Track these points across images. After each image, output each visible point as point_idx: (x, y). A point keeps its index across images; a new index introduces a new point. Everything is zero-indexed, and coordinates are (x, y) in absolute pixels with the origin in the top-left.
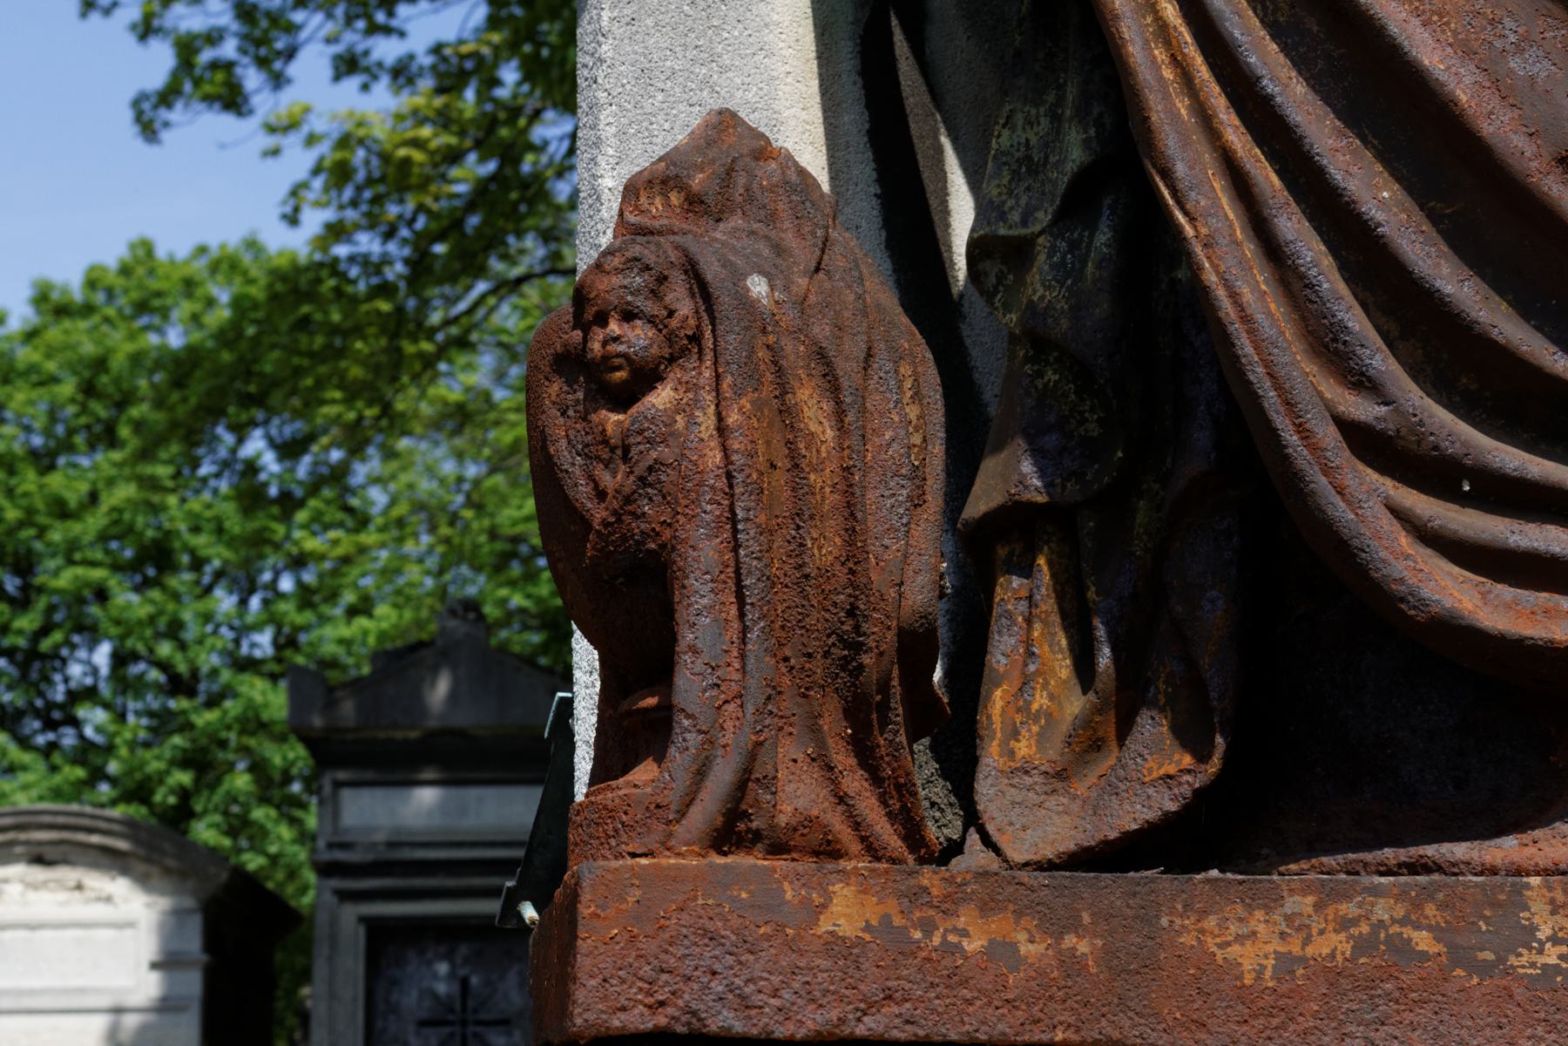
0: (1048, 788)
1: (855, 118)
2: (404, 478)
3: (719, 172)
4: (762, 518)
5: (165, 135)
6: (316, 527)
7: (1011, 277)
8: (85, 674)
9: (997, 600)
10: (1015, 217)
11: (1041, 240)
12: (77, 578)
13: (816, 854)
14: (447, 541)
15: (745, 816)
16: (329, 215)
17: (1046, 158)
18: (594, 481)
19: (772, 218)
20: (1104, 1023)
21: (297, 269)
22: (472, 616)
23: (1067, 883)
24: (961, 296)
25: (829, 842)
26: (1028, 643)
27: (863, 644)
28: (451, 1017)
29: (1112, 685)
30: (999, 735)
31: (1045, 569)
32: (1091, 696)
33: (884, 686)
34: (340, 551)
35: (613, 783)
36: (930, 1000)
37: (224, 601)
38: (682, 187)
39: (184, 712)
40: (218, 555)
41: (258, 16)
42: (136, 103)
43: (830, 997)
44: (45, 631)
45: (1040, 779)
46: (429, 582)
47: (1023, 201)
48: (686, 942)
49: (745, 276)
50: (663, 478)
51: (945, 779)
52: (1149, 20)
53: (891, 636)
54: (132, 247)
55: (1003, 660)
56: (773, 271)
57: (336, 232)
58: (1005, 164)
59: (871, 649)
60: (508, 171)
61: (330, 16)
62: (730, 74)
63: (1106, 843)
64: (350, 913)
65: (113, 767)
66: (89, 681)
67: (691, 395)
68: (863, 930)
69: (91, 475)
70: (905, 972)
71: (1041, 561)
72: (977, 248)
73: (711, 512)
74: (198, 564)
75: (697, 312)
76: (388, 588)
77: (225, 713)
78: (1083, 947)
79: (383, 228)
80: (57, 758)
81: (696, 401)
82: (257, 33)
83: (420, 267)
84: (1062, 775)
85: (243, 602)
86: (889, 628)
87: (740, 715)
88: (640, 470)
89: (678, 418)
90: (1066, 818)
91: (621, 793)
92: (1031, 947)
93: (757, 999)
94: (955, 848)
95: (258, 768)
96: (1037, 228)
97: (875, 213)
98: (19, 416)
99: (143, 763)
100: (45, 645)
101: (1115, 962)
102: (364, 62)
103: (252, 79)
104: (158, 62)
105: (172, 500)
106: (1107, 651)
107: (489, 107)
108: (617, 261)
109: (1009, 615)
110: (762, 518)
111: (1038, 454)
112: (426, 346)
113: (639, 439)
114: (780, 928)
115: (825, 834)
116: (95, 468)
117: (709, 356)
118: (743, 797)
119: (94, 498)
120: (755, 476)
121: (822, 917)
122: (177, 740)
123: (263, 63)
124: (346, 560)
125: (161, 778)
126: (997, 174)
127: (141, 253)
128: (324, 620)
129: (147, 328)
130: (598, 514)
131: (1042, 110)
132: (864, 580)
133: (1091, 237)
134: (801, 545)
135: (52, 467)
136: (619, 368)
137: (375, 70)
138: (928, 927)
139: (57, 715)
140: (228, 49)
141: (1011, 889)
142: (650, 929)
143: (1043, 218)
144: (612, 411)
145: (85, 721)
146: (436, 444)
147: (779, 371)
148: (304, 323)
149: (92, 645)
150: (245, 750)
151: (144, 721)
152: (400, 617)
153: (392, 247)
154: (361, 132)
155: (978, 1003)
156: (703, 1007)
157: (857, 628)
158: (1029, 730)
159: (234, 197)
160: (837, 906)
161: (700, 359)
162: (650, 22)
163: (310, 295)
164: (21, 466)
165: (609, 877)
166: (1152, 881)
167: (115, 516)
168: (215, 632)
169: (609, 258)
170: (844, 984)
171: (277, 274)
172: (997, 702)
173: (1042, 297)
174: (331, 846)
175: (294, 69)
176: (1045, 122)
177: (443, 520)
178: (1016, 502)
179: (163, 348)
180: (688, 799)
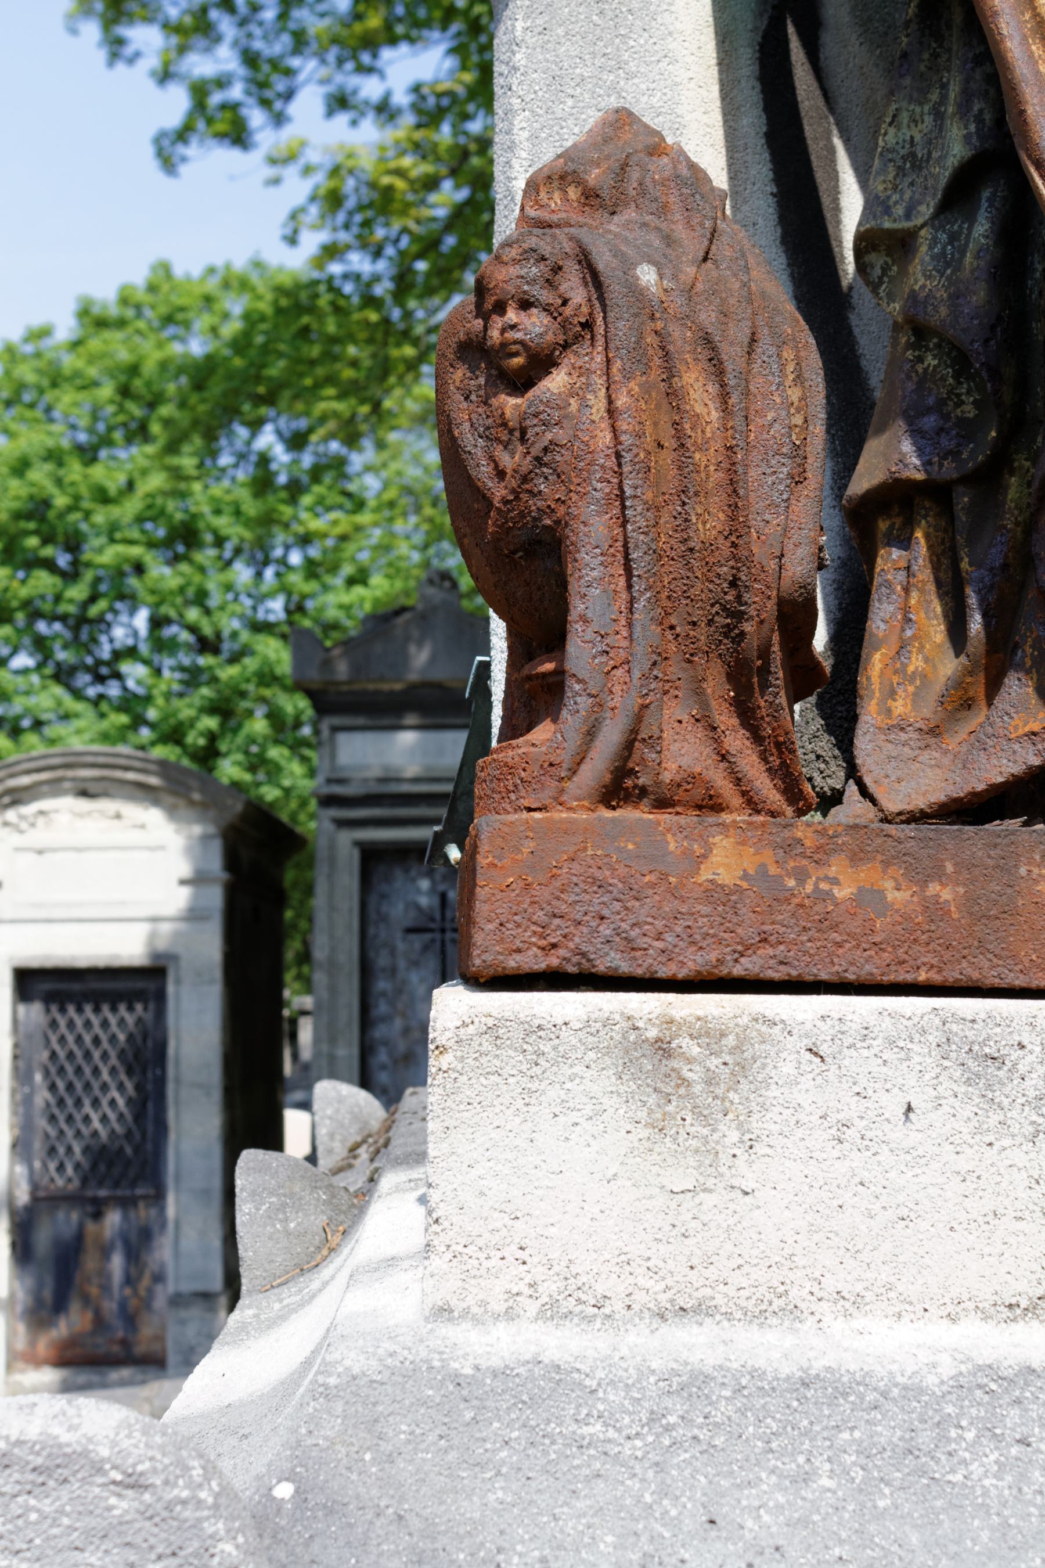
0: (922, 744)
1: (753, 121)
2: (394, 466)
3: (617, 168)
4: (649, 496)
5: (183, 169)
6: (319, 509)
7: (895, 268)
8: (127, 636)
9: (878, 570)
10: (899, 211)
11: (923, 233)
12: (117, 555)
13: (699, 807)
14: (430, 520)
15: (632, 772)
16: (323, 237)
17: (930, 153)
18: (494, 461)
19: (663, 210)
20: (964, 964)
21: (298, 286)
22: (447, 584)
23: (931, 835)
24: (851, 288)
25: (711, 797)
26: (906, 610)
27: (744, 613)
28: (432, 926)
29: (982, 649)
30: (877, 695)
31: (922, 541)
32: (963, 658)
33: (764, 653)
34: (338, 530)
35: (514, 742)
36: (802, 943)
37: (242, 573)
38: (579, 182)
39: (210, 668)
40: (235, 532)
41: (260, 62)
42: (158, 140)
43: (710, 940)
44: (93, 599)
45: (915, 735)
46: (416, 557)
47: (907, 195)
48: (576, 889)
49: (635, 265)
50: (558, 458)
51: (830, 734)
52: (1027, 16)
53: (771, 606)
54: (154, 268)
55: (883, 626)
56: (663, 261)
57: (331, 252)
58: (890, 160)
59: (752, 618)
60: (480, 196)
61: (323, 61)
62: (636, 81)
63: (974, 794)
64: (346, 838)
65: (152, 714)
66: (130, 642)
67: (583, 379)
68: (741, 879)
69: (128, 466)
70: (780, 917)
71: (919, 534)
72: (865, 242)
73: (601, 489)
74: (219, 541)
75: (589, 300)
76: (384, 561)
77: (244, 668)
78: (946, 895)
79: (372, 249)
80: (104, 706)
81: (588, 385)
82: (260, 77)
83: (404, 283)
84: (935, 731)
85: (259, 575)
86: (769, 598)
87: (627, 680)
88: (536, 451)
89: (572, 401)
90: (939, 771)
91: (520, 751)
92: (897, 894)
93: (642, 942)
94: (831, 800)
95: (275, 717)
96: (920, 221)
97: (771, 210)
98: (66, 416)
99: (175, 714)
100: (94, 611)
101: (976, 908)
102: (353, 101)
103: (256, 117)
104: (175, 105)
105: (197, 487)
106: (978, 617)
107: (462, 140)
108: (514, 252)
109: (889, 584)
110: (649, 496)
111: (916, 433)
112: (409, 351)
113: (535, 421)
114: (664, 876)
115: (708, 789)
116: (132, 459)
117: (600, 342)
118: (630, 755)
119: (130, 486)
120: (642, 455)
121: (702, 867)
122: (205, 691)
123: (265, 103)
124: (344, 538)
125: (192, 723)
126: (883, 170)
127: (161, 273)
128: (326, 588)
129: (174, 338)
130: (499, 492)
131: (926, 108)
132: (746, 553)
133: (970, 229)
134: (686, 520)
135: (94, 459)
136: (516, 354)
137: (362, 107)
138: (801, 876)
139: (104, 671)
140: (236, 92)
141: (879, 841)
142: (543, 878)
143: (926, 211)
144: (509, 395)
145: (128, 675)
146: (420, 436)
147: (667, 355)
148: (305, 332)
149: (133, 611)
150: (263, 700)
151: (178, 675)
152: (392, 585)
153: (381, 266)
154: (350, 163)
155: (847, 946)
156: (592, 949)
157: (739, 598)
158: (905, 691)
159: (244, 222)
160: (717, 857)
161: (592, 345)
162: (561, 31)
163: (311, 309)
164: (67, 459)
165: (506, 829)
166: (1013, 833)
167: (149, 501)
168: (236, 599)
169: (507, 249)
170: (723, 928)
171: (280, 290)
172: (876, 665)
173: (923, 287)
174: (329, 781)
175: (293, 109)
176: (928, 120)
177: (426, 502)
178: (896, 480)
179: (186, 355)
180: (579, 758)
